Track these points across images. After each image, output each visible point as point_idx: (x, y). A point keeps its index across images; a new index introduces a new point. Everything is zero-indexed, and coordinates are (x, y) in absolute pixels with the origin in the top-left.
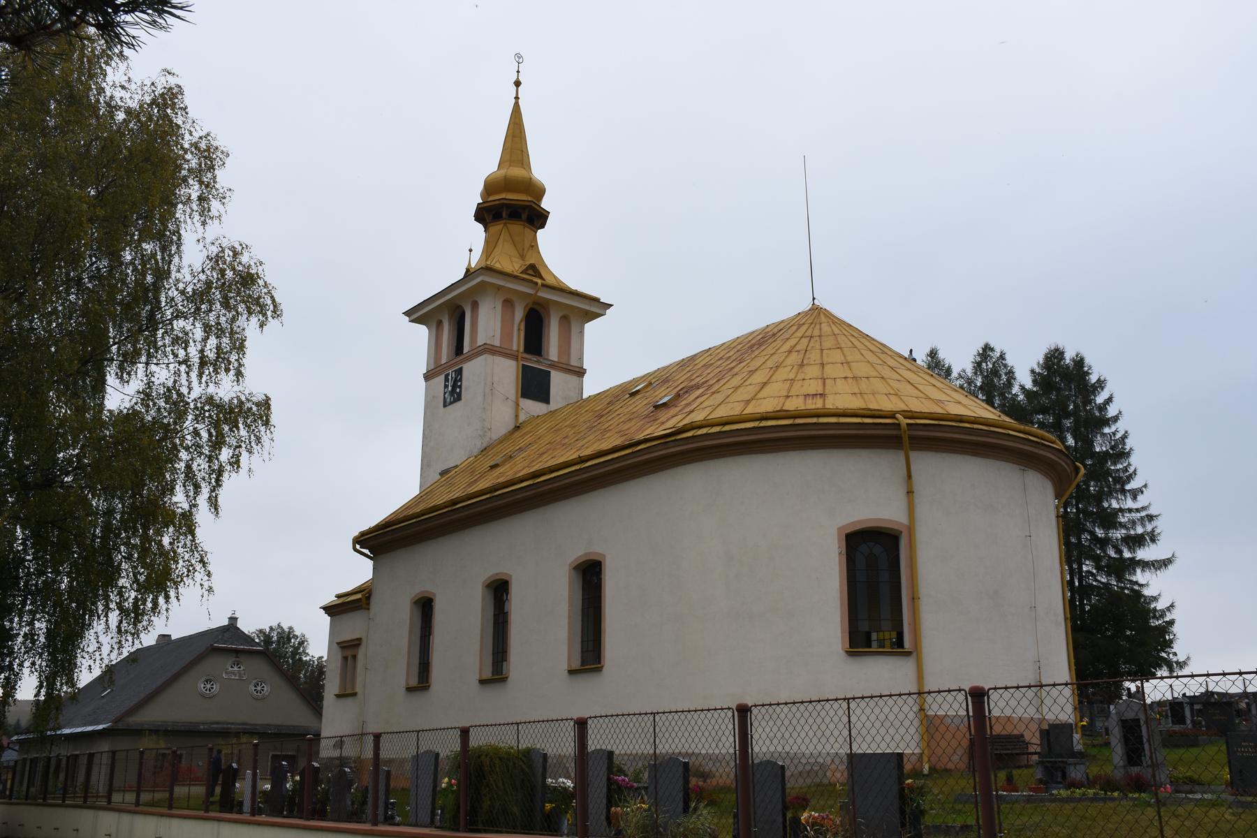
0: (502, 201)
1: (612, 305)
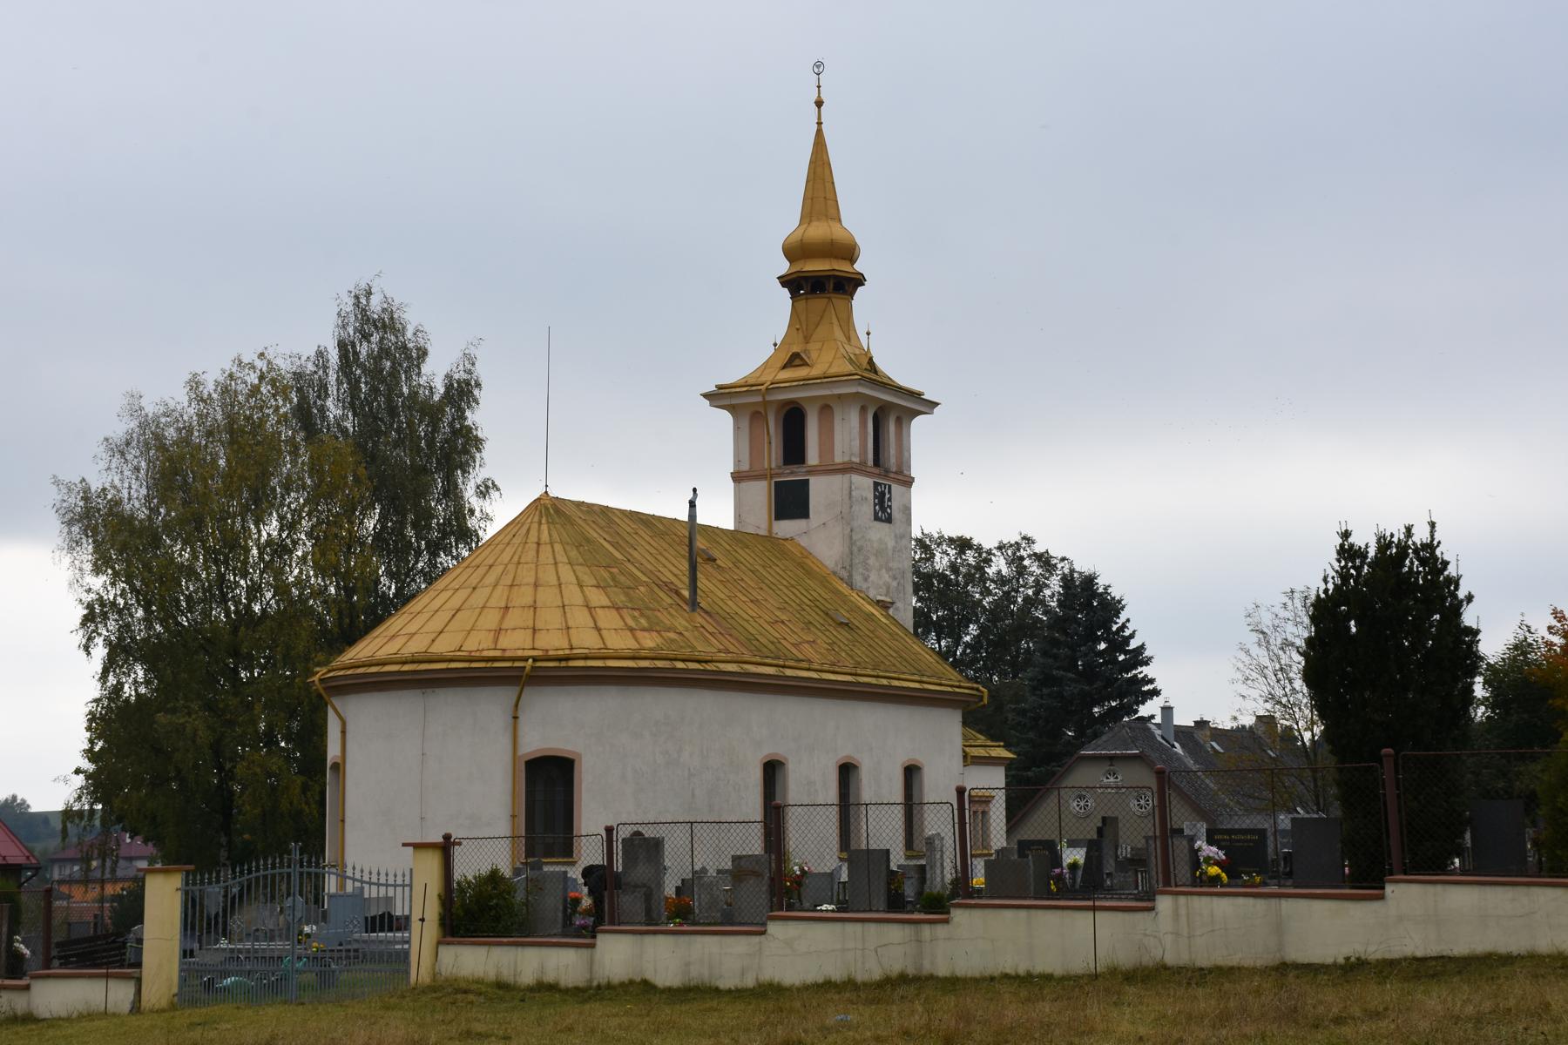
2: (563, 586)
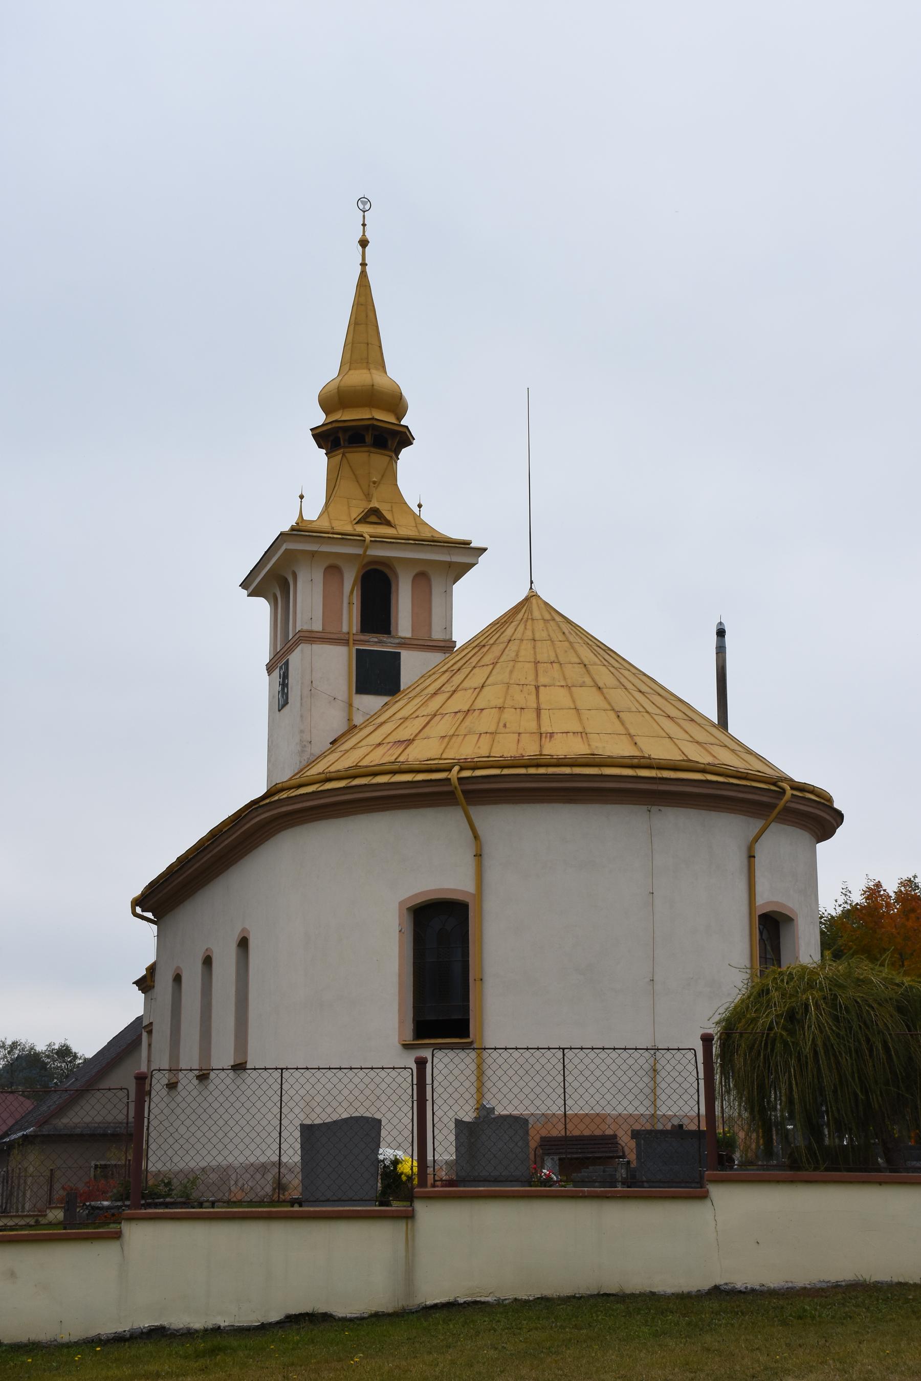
0: (334, 425)
1: (485, 550)
2: (544, 714)
